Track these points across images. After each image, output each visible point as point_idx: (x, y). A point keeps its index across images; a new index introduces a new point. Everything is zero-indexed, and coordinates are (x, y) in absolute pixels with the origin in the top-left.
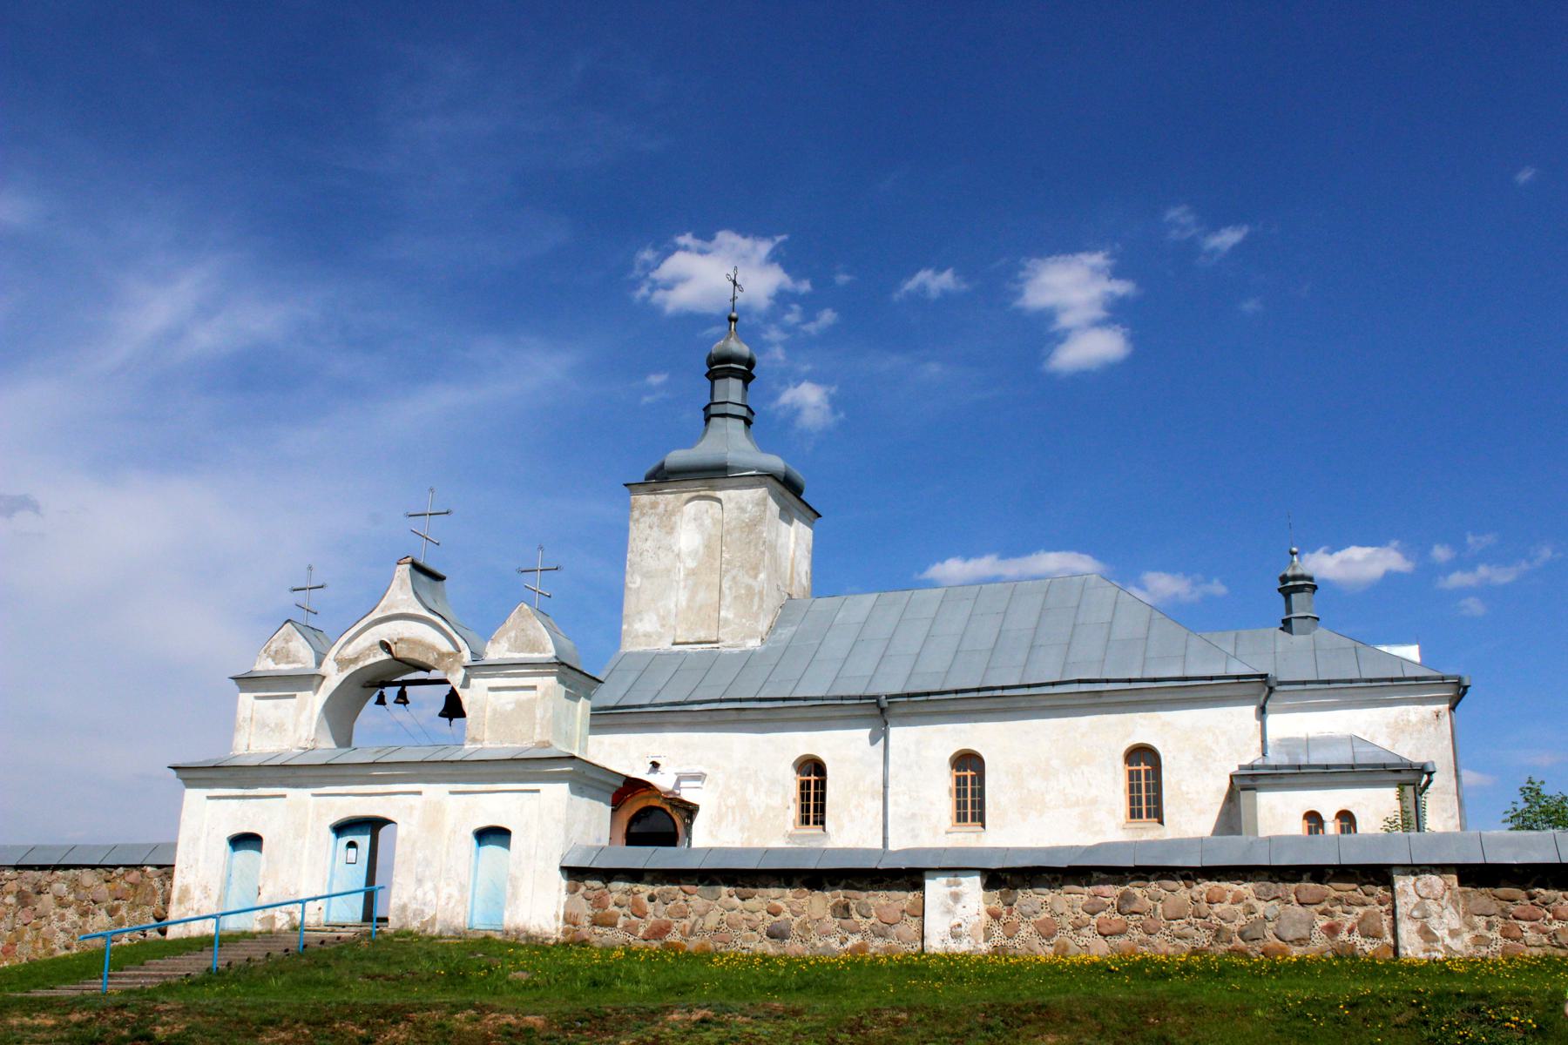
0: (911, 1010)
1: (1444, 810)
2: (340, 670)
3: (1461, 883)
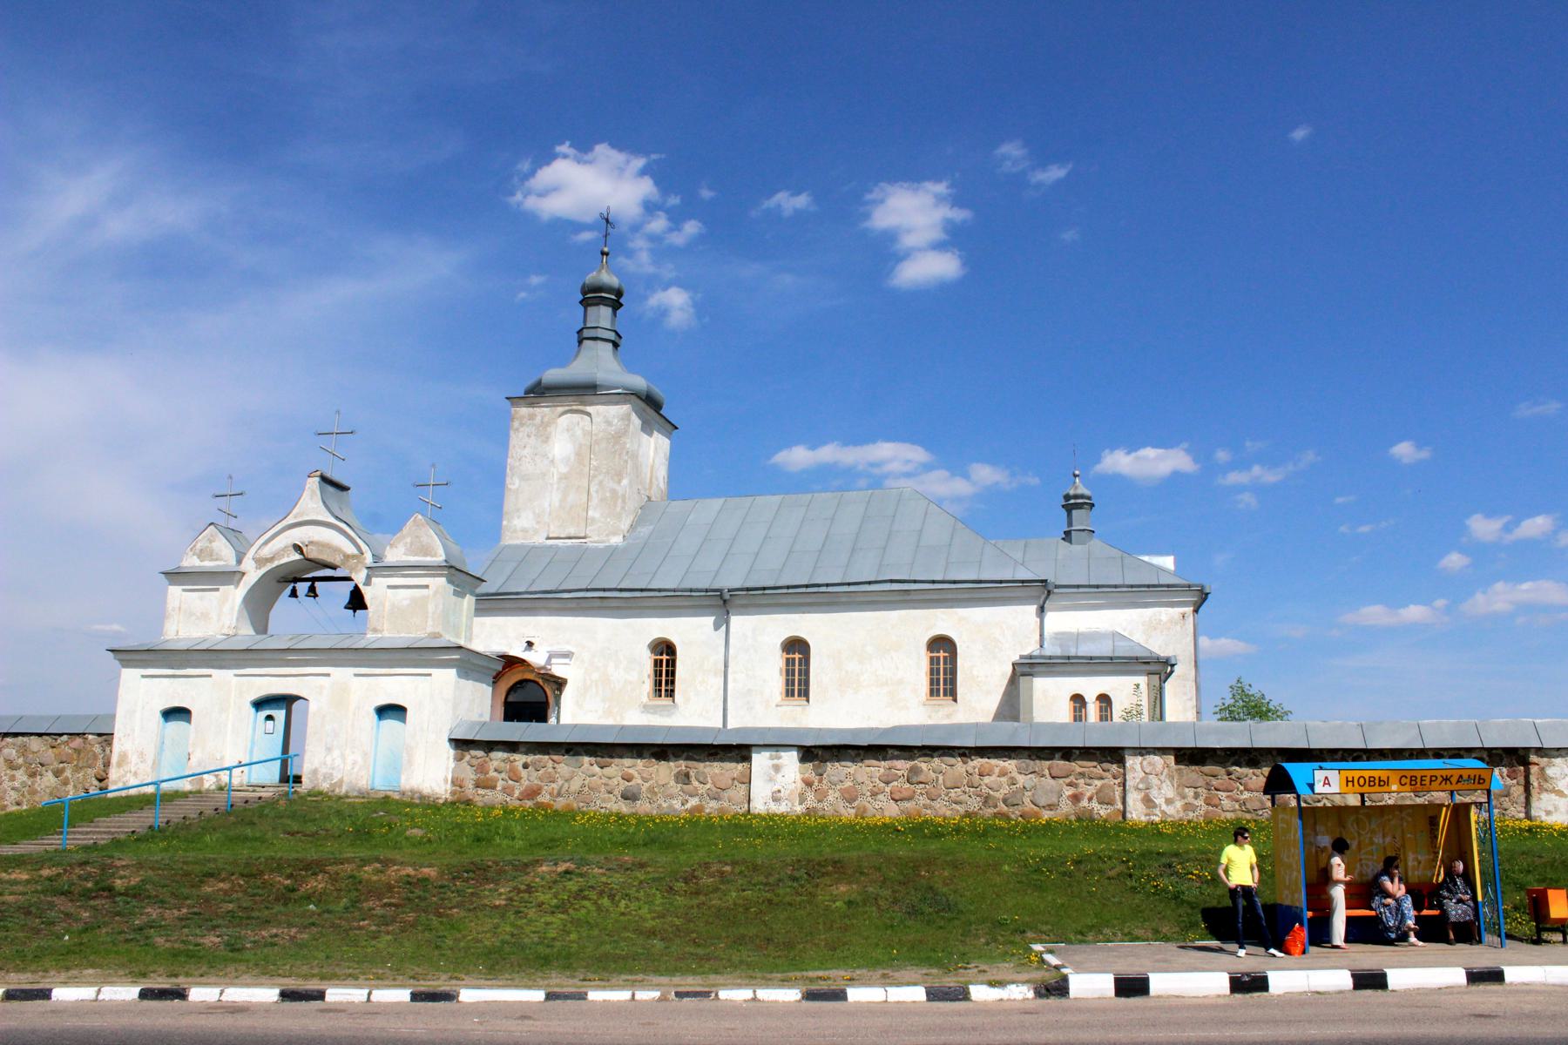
0: (734, 863)
2: (258, 567)
3: (1178, 762)
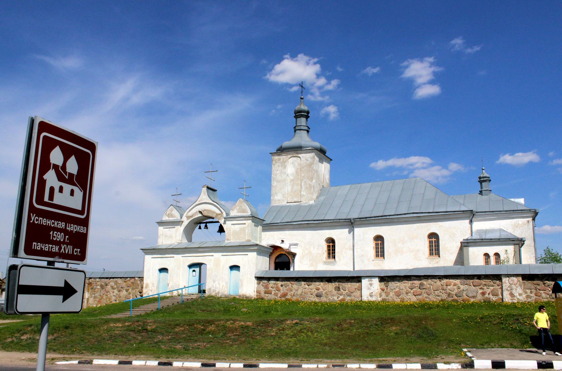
0: (355, 319)
1: (530, 252)
3: (523, 279)
